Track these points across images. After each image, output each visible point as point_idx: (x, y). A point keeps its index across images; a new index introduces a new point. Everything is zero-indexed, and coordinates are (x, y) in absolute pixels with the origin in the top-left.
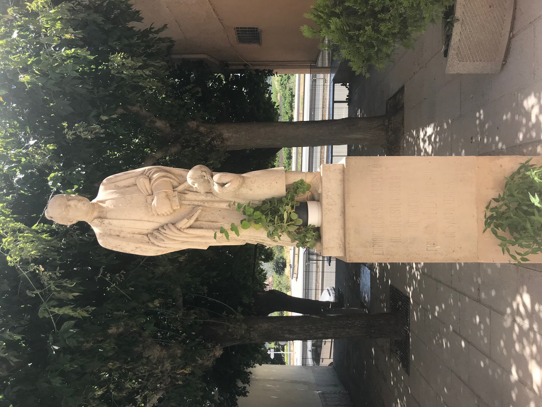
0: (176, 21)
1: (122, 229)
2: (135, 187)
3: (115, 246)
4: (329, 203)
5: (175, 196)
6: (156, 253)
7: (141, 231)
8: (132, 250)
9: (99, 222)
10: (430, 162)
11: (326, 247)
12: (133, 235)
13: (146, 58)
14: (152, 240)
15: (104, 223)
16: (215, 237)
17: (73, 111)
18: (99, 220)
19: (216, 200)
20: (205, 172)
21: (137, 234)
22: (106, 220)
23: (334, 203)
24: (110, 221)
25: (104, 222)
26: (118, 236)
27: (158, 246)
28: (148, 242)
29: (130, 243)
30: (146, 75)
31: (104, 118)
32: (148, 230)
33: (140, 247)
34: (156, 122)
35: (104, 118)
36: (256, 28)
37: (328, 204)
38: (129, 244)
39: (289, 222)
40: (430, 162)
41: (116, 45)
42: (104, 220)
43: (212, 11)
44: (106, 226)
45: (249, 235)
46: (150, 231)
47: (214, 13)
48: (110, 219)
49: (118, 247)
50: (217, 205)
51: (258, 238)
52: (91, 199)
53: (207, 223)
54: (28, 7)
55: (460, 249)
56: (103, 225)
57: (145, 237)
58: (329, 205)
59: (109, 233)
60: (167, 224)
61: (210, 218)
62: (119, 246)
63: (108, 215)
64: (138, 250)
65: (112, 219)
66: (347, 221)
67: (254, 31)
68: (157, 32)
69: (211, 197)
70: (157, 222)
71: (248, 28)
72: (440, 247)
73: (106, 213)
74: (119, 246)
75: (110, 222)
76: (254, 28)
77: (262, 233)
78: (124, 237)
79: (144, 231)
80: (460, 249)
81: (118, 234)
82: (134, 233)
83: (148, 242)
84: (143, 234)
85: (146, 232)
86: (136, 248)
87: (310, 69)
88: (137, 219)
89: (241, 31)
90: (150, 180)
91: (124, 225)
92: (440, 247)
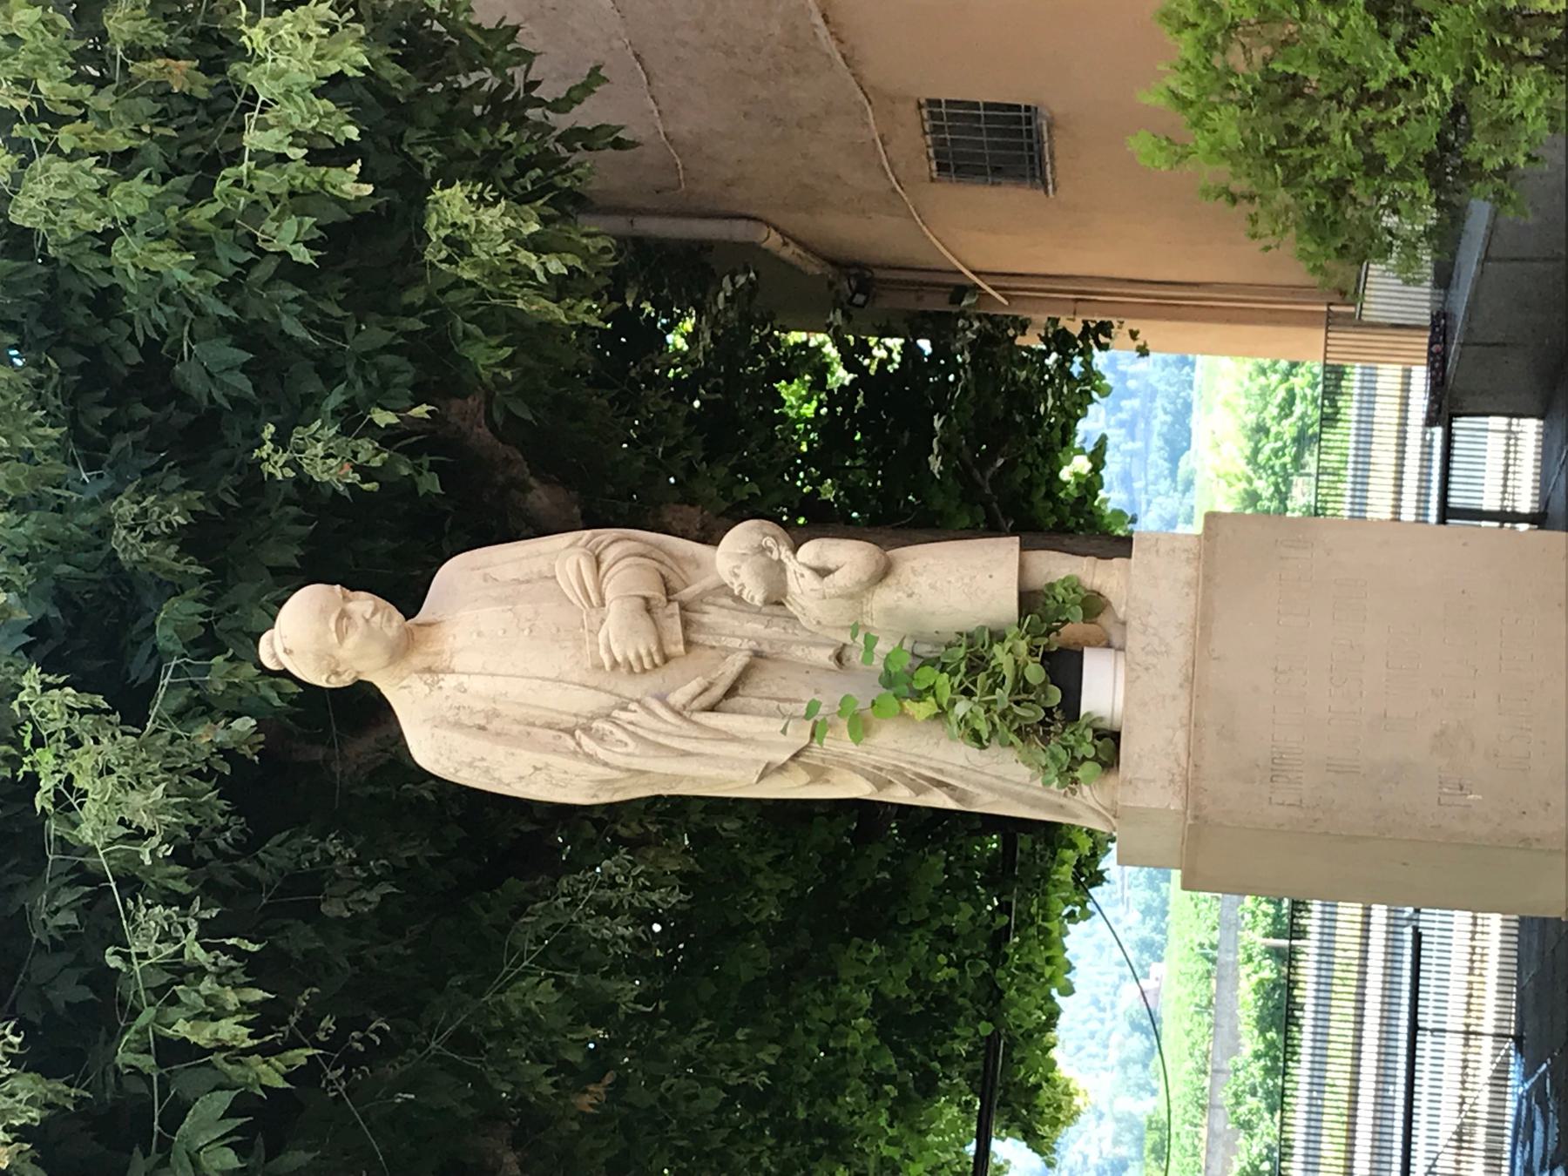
0: (637, 56)
1: (499, 707)
2: (551, 584)
3: (469, 760)
4: (1149, 648)
5: (672, 616)
6: (592, 792)
7: (557, 718)
8: (521, 778)
9: (425, 683)
10: (1465, 544)
11: (1129, 776)
12: (529, 729)
13: (552, 211)
14: (588, 744)
15: (440, 688)
16: (784, 731)
17: (251, 392)
18: (427, 676)
19: (799, 638)
20: (774, 537)
21: (541, 726)
22: (448, 677)
23: (1164, 649)
24: (464, 678)
25: (441, 683)
26: (482, 728)
27: (606, 764)
28: (575, 753)
29: (518, 751)
30: (547, 273)
31: (383, 418)
32: (576, 715)
33: (547, 765)
34: (531, 488)
35: (383, 418)
36: (1028, 108)
37: (1143, 649)
38: (513, 754)
39: (1019, 693)
40: (1465, 544)
41: (425, 155)
42: (441, 676)
43: (819, 21)
44: (447, 697)
45: (894, 746)
46: (582, 721)
47: (823, 31)
48: (463, 673)
49: (477, 763)
50: (799, 653)
51: (922, 761)
52: (407, 618)
53: (765, 701)
54: (244, 39)
55: (1546, 810)
56: (436, 693)
57: (567, 738)
58: (1147, 654)
59: (452, 719)
60: (644, 671)
61: (774, 689)
62: (483, 759)
63: (457, 663)
64: (541, 776)
65: (469, 674)
66: (932, 267)
67: (1018, 120)
68: (561, 105)
69: (784, 628)
70: (610, 692)
71: (988, 106)
72: (1480, 797)
73: (452, 656)
74: (483, 759)
75: (461, 684)
76: (1017, 107)
77: (937, 744)
78: (498, 734)
79: (564, 717)
80: (1546, 810)
81: (483, 722)
82: (533, 724)
83: (575, 753)
84: (560, 730)
85: (569, 721)
86: (536, 769)
87: (1323, 331)
88: (547, 675)
89: (951, 117)
90: (598, 562)
91: (506, 694)
92: (1480, 797)
